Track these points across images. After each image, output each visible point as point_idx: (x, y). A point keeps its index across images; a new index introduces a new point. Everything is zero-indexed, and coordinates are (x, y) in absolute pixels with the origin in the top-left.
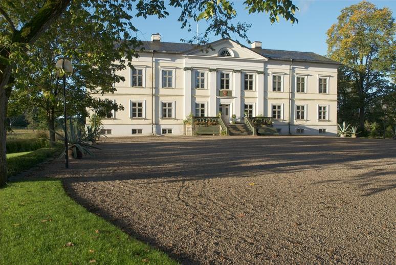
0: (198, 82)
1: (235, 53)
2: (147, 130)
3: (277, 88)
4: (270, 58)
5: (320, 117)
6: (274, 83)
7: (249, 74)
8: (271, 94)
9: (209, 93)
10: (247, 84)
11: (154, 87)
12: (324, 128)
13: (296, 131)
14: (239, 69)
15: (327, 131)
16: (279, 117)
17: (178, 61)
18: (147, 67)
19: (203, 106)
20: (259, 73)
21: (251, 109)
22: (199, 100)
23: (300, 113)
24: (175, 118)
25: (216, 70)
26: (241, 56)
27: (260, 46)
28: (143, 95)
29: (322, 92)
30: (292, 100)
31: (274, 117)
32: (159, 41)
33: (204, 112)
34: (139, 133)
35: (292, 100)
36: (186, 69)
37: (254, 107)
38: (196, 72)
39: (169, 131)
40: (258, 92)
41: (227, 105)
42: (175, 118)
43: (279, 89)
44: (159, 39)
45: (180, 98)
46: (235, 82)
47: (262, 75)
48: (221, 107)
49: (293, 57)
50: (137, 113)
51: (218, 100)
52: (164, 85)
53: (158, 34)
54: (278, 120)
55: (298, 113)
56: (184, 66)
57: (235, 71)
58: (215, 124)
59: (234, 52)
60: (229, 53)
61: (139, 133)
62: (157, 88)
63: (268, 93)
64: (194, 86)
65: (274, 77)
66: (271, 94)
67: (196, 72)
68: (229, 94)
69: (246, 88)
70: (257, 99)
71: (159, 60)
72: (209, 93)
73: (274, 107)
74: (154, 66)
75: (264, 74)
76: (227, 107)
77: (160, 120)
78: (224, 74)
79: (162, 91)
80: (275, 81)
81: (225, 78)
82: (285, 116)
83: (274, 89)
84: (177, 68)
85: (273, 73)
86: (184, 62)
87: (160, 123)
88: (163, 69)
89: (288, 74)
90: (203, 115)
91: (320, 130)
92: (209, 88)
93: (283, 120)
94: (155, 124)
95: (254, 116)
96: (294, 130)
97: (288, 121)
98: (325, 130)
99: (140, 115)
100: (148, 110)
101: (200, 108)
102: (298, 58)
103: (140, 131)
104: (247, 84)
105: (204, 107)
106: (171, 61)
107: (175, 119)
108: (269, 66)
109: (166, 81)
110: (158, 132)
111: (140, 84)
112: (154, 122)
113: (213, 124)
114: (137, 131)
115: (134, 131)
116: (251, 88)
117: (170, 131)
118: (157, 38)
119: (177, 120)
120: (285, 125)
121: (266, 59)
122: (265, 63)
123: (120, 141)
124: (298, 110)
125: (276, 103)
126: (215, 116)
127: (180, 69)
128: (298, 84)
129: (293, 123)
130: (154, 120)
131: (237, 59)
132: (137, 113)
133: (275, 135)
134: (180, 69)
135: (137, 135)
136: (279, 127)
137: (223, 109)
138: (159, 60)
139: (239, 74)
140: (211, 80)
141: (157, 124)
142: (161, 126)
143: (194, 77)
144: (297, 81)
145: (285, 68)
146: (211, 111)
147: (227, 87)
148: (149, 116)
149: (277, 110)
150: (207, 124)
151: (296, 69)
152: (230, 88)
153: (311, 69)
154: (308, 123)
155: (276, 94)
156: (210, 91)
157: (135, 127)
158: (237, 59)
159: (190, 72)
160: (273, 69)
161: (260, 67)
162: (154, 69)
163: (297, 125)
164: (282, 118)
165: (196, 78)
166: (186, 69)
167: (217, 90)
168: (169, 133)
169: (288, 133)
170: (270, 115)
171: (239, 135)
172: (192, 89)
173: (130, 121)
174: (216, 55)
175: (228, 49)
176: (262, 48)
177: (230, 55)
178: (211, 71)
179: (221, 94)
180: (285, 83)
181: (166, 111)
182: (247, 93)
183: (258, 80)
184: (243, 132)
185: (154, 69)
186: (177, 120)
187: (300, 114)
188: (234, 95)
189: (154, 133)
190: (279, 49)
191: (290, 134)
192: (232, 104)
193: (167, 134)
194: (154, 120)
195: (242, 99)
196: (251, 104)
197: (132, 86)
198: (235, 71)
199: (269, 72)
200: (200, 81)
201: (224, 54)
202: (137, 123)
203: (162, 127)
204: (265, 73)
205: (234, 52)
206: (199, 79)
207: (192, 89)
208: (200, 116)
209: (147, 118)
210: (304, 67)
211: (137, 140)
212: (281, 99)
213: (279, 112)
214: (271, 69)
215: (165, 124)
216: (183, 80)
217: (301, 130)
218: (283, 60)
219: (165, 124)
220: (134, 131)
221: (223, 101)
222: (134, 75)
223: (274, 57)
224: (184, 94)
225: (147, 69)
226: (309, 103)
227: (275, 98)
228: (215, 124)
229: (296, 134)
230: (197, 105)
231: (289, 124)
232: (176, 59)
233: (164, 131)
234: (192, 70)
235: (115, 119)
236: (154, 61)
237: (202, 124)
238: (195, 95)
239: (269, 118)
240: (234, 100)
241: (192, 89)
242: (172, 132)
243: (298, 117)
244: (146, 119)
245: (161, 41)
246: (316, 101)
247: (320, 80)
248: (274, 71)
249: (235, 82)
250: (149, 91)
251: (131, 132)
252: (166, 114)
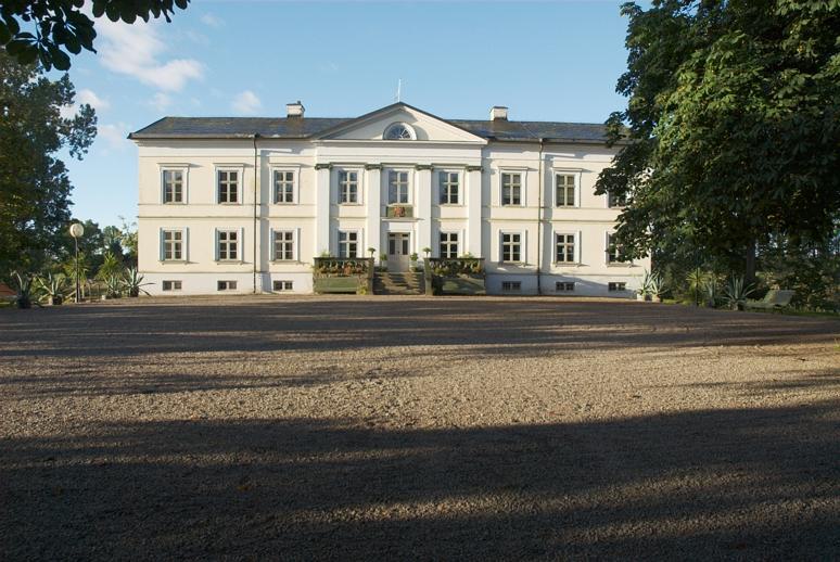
0: (343, 189)
1: (418, 131)
2: (246, 284)
3: (511, 197)
4: (492, 139)
5: (223, 255)
6: (505, 188)
7: (348, 170)
8: (498, 210)
9: (466, 212)
10: (446, 193)
11: (258, 201)
12: (622, 280)
13: (554, 287)
14: (327, 162)
15: (627, 287)
16: (517, 257)
17: (306, 152)
18: (245, 166)
19: (353, 236)
20: (470, 169)
21: (353, 242)
22: (345, 227)
23: (564, 249)
24: (299, 260)
25: (381, 167)
26: (433, 137)
27: (504, 115)
28: (238, 218)
29: (508, 203)
30: (545, 222)
31: (506, 257)
32: (300, 116)
33: (456, 250)
34: (231, 288)
35: (545, 222)
36: (319, 167)
37: (460, 238)
38: (440, 173)
39: (287, 284)
40: (468, 209)
41: (406, 235)
42: (299, 260)
43: (517, 201)
44: (299, 112)
45: (306, 221)
46: (420, 189)
47: (479, 173)
48: (392, 238)
49: (545, 135)
50: (511, 253)
51: (383, 225)
52: (278, 199)
53: (299, 103)
54: (512, 265)
55: (560, 249)
56: (316, 161)
57: (419, 168)
58: (359, 272)
59: (417, 129)
60: (406, 132)
61: (231, 288)
62: (547, 208)
63: (492, 210)
64: (437, 199)
65: (505, 177)
66: (498, 210)
67: (440, 173)
68: (406, 213)
69: (443, 200)
70: (467, 223)
71: (552, 156)
72: (466, 212)
73: (506, 238)
74: (543, 168)
75: (483, 172)
76: (406, 238)
77: (271, 264)
78: (345, 173)
79: (275, 210)
80: (561, 186)
81: (348, 183)
82: (531, 256)
83: (506, 201)
84: (302, 166)
85: (501, 168)
86: (317, 153)
87: (270, 270)
88: (220, 169)
89: (535, 170)
90: (353, 255)
91: (612, 286)
92: (467, 203)
93: (526, 264)
94: (261, 272)
95: (359, 255)
96: (550, 284)
97: (536, 268)
98: (622, 284)
99: (233, 255)
100: (248, 247)
101: (348, 241)
102: (553, 134)
103: (233, 285)
104: (446, 193)
105: (456, 240)
106: (293, 152)
107: (299, 262)
108: (493, 155)
109: (345, 191)
110: (265, 287)
111: (234, 198)
112: (258, 269)
113: (354, 272)
114: (228, 284)
115: (222, 285)
116: (455, 200)
117: (289, 285)
118: (501, 114)
119: (304, 264)
120: (530, 274)
121: (485, 142)
122: (483, 148)
123: (194, 309)
124: (560, 244)
125: (510, 229)
126: (479, 256)
127: (308, 166)
128: (560, 190)
129: (549, 269)
130: (258, 263)
131: (423, 143)
132: (511, 253)
133: (478, 295)
134: (308, 166)
135: (228, 292)
136: (517, 279)
137: (395, 244)
138: (552, 156)
139: (428, 173)
140: (369, 187)
141: (264, 272)
142: (272, 275)
143: (437, 182)
144: (558, 184)
145: (530, 158)
146: (369, 246)
147: (405, 199)
148: (249, 258)
149: (511, 243)
150: (343, 271)
151: (272, 154)
152: (410, 202)
153: (588, 157)
154: (582, 270)
155: (510, 211)
156: (366, 208)
157: (223, 278)
158: (423, 143)
159: (326, 172)
160: (502, 160)
161: (474, 157)
162: (259, 169)
163: (557, 275)
164: (523, 259)
165: (440, 185)
166: (319, 167)
167: (381, 205)
168: (286, 288)
169: (536, 292)
170: (495, 256)
171: (399, 293)
172: (432, 206)
173: (214, 266)
174: (381, 137)
175: (404, 124)
176: (509, 119)
177: (409, 136)
178: (368, 169)
179: (389, 212)
180: (531, 188)
181: (283, 246)
182: (446, 210)
183: (469, 185)
184: (412, 288)
185: (259, 169)
186: (304, 264)
187: (565, 251)
188: (416, 214)
189: (259, 289)
190: (325, 117)
191: (540, 293)
192: (464, 231)
193: (284, 292)
194: (258, 263)
195: (435, 222)
196: (454, 232)
197: (164, 203)
198: (419, 168)
199: (494, 166)
200: (229, 189)
201: (396, 134)
202: (227, 271)
203: (274, 278)
204: (483, 169)
205: (417, 129)
206: (345, 186)
207: (331, 205)
208: (348, 256)
209: (246, 260)
210: (290, 150)
211: (168, 300)
212: (521, 220)
213: (517, 248)
214: (498, 162)
215: (279, 271)
216: (314, 189)
217: (566, 286)
218: (560, 143)
219: (279, 271)
220: (222, 285)
221: (396, 227)
222: (223, 182)
223: (501, 134)
224: (316, 215)
225: (247, 169)
226: (585, 228)
227: (505, 219)
228: (359, 272)
229: (554, 293)
230: (342, 235)
231: (539, 273)
232: (301, 149)
233: (278, 285)
234: (382, 170)
235: (188, 262)
236: (259, 153)
237: (334, 272)
238: (267, 216)
239: (477, 259)
240: (417, 224)
241: (331, 205)
242: (293, 286)
243: (560, 258)
244: (243, 262)
245: (306, 115)
246: (600, 225)
247: (222, 176)
248: (505, 163)
249: (420, 189)
250: (248, 211)
251: (216, 286)
252: (515, 250)
